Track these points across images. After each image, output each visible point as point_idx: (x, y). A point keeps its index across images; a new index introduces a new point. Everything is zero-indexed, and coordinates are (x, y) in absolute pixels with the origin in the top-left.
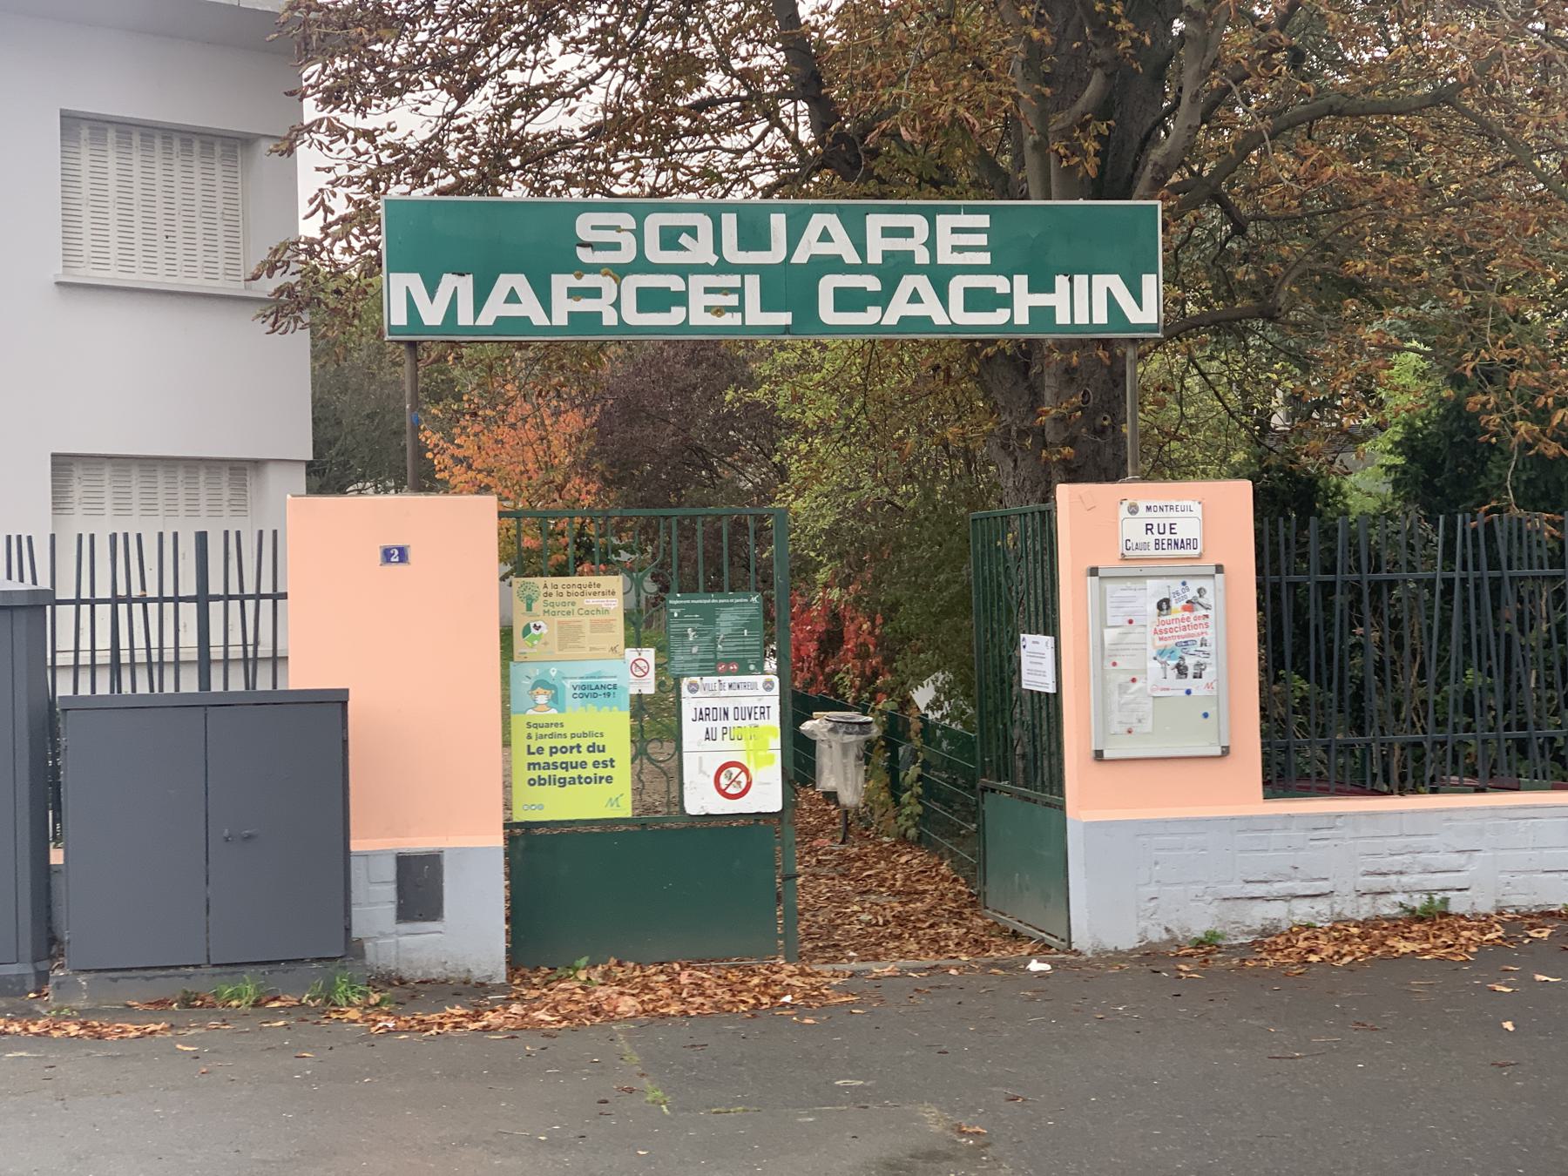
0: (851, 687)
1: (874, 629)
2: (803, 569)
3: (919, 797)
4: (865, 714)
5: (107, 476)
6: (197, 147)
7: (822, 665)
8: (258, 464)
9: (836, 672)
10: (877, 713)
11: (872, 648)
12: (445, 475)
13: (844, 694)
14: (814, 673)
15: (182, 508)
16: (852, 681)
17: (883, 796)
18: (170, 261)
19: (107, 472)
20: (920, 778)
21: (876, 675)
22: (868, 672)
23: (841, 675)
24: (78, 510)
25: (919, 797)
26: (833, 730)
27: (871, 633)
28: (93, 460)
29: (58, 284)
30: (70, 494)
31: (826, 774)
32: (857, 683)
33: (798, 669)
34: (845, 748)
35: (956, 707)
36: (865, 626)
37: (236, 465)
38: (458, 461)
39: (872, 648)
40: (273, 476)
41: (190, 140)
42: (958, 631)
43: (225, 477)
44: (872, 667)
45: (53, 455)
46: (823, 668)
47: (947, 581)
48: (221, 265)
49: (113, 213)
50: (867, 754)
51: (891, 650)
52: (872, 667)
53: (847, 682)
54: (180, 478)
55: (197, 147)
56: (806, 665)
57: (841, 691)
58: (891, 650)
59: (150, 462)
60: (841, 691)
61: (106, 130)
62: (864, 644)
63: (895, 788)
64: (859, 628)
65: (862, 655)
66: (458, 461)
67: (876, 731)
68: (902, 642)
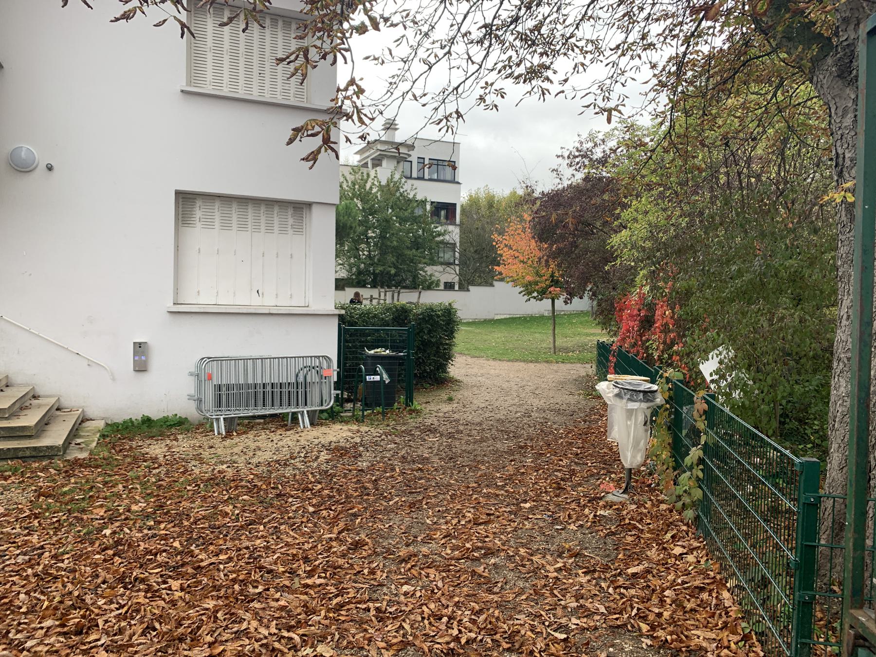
0: (657, 350)
1: (674, 314)
2: (628, 277)
3: (698, 479)
4: (653, 382)
5: (217, 207)
6: (280, 23)
7: (641, 336)
8: (309, 205)
9: (648, 340)
10: (663, 380)
11: (671, 326)
12: (501, 252)
13: (653, 353)
14: (636, 340)
15: (263, 227)
16: (658, 347)
17: (665, 455)
18: (248, 80)
19: (217, 204)
20: (701, 461)
21: (673, 344)
22: (668, 341)
23: (650, 342)
24: (199, 225)
25: (698, 479)
26: (618, 396)
27: (672, 318)
28: (208, 197)
29: (182, 91)
30: (194, 216)
31: (616, 428)
32: (661, 347)
33: (627, 336)
34: (630, 413)
35: (738, 378)
36: (667, 313)
37: (298, 206)
38: (506, 246)
39: (671, 326)
40: (316, 211)
41: (277, 20)
42: (744, 314)
43: (290, 211)
44: (671, 339)
45: (178, 193)
46: (641, 337)
47: (739, 270)
48: (292, 92)
49: (226, 58)
50: (651, 422)
51: (683, 326)
52: (671, 339)
53: (654, 346)
54: (276, 212)
55: (280, 23)
56: (631, 335)
57: (650, 352)
58: (683, 326)
59: (244, 201)
60: (650, 352)
61: (223, 9)
62: (666, 324)
63: (678, 450)
64: (664, 314)
65: (665, 330)
66: (506, 246)
67: (659, 400)
68: (692, 321)
